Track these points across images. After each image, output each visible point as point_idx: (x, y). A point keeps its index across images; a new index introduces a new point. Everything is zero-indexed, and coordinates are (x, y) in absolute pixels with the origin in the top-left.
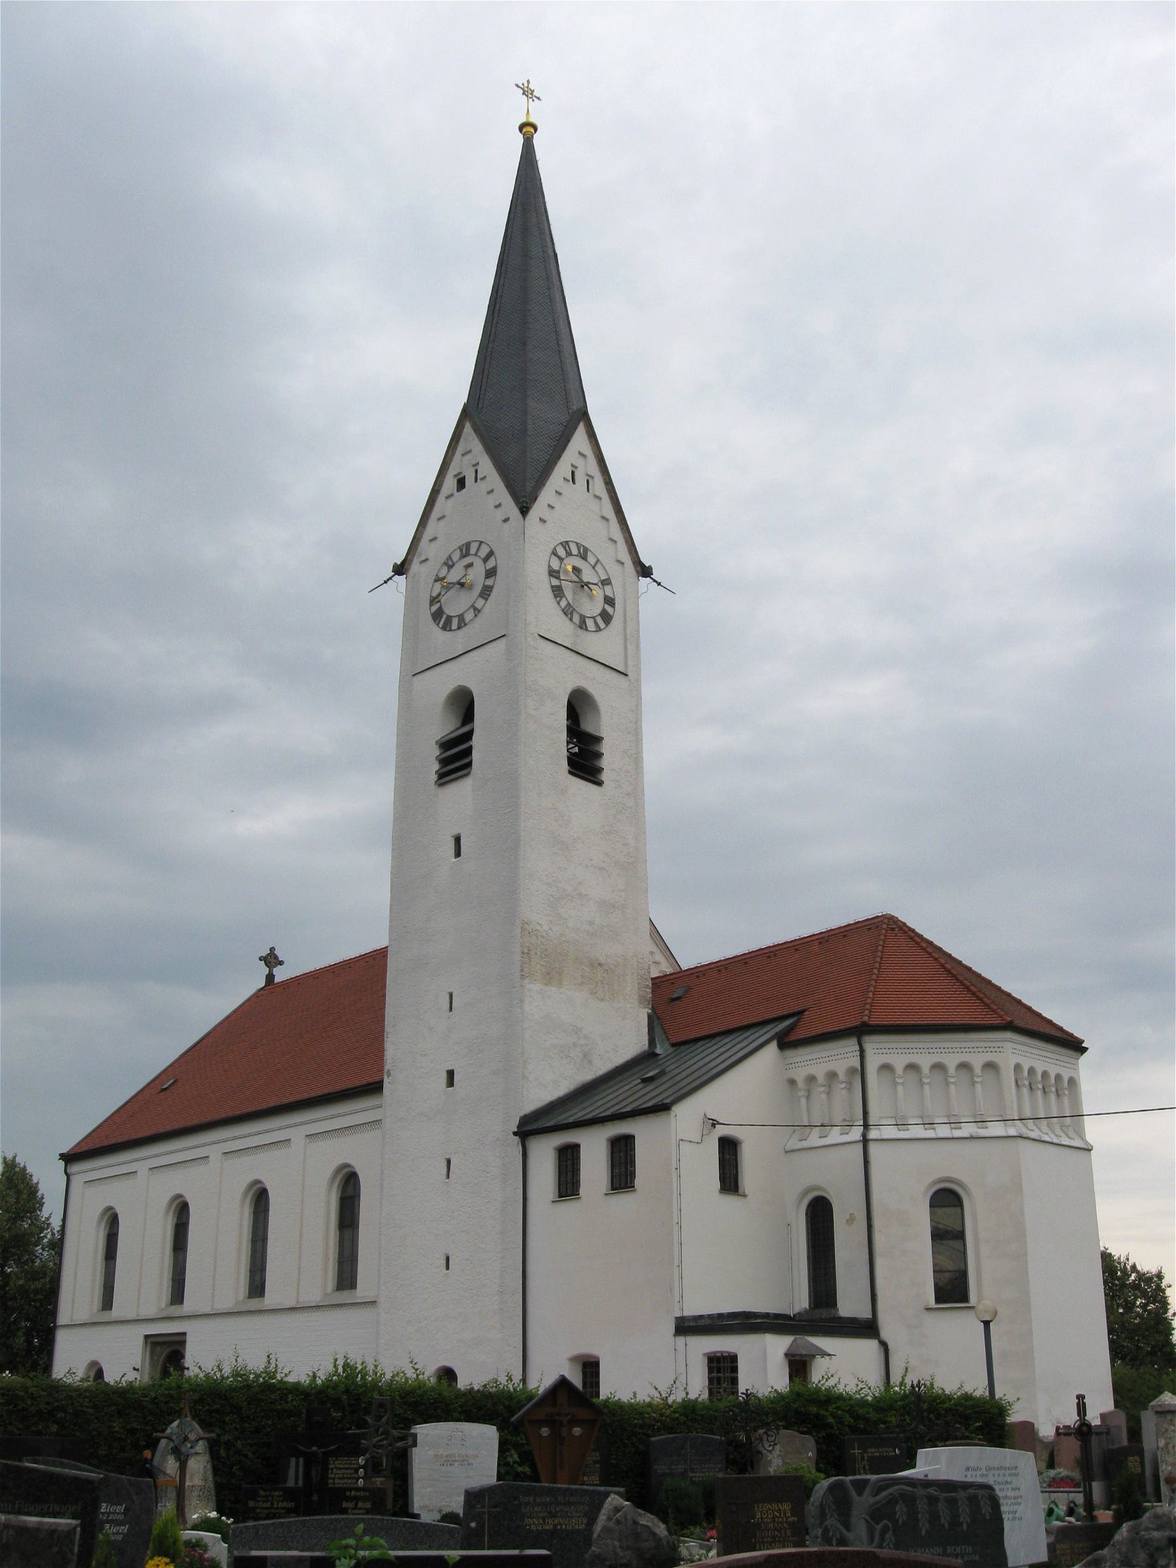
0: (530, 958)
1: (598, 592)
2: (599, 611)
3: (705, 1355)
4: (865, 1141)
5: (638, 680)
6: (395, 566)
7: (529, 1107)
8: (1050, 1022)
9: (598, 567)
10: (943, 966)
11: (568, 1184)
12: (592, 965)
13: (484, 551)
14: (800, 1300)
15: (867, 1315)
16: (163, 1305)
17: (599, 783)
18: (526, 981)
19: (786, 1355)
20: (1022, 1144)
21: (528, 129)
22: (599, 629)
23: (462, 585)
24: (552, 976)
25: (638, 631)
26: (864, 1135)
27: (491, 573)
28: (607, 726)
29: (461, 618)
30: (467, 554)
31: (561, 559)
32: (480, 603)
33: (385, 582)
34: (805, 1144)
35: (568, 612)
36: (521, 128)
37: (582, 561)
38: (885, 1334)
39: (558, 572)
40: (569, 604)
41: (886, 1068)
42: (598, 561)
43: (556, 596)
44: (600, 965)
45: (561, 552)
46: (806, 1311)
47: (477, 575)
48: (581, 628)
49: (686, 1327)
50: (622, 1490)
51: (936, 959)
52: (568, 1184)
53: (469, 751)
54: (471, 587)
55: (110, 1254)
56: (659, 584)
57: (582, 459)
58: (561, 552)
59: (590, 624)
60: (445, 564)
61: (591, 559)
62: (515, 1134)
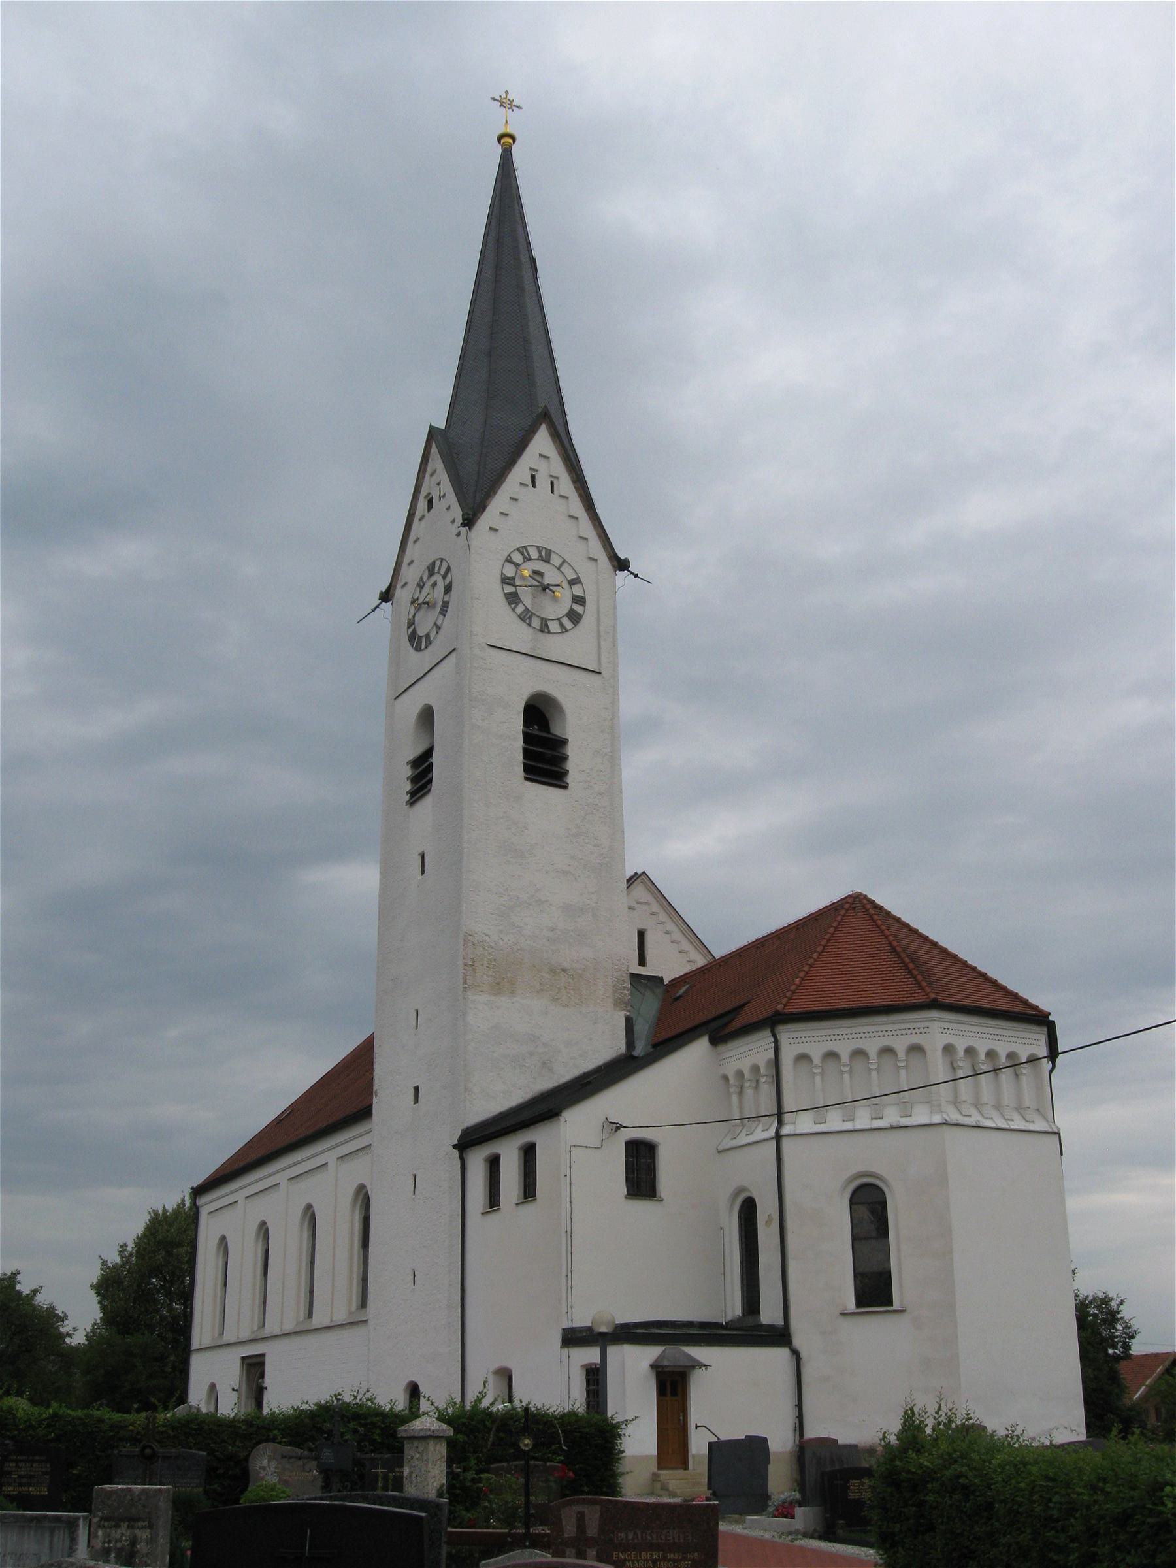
0: (474, 970)
1: (564, 596)
2: (566, 611)
3: (583, 1366)
4: (778, 1137)
5: (615, 677)
6: (381, 594)
7: (472, 1120)
8: (1015, 996)
9: (565, 568)
10: (890, 943)
12: (553, 971)
14: (734, 1309)
15: (780, 1322)
16: (354, 1308)
17: (565, 787)
18: (469, 993)
19: (652, 1366)
20: (948, 1132)
21: (506, 140)
22: (564, 630)
23: (427, 603)
24: (503, 985)
25: (614, 627)
26: (777, 1132)
27: (448, 589)
28: (576, 730)
29: (427, 636)
31: (517, 565)
33: (373, 611)
34: (734, 1143)
35: (526, 617)
36: (499, 139)
37: (545, 564)
38: (797, 1342)
39: (514, 578)
40: (527, 609)
41: (803, 1058)
42: (564, 561)
43: (510, 603)
44: (564, 970)
45: (517, 558)
46: (739, 1319)
47: (438, 594)
48: (542, 631)
49: (573, 1338)
51: (886, 937)
53: (430, 766)
54: (434, 606)
55: (312, 1262)
56: (636, 576)
57: (543, 461)
58: (517, 558)
59: (554, 627)
60: (418, 585)
61: (556, 560)
62: (455, 1147)
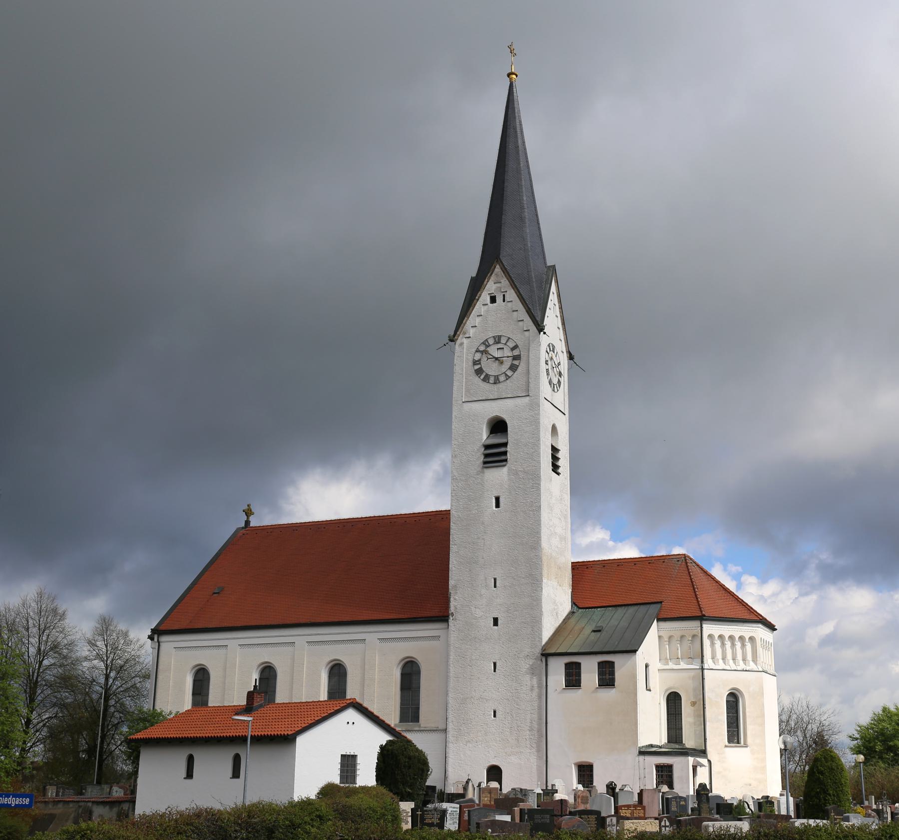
4: (703, 669)
11: (573, 679)
13: (511, 344)
27: (517, 358)
30: (499, 342)
32: (509, 373)
41: (711, 636)
50: (162, 788)
52: (573, 679)
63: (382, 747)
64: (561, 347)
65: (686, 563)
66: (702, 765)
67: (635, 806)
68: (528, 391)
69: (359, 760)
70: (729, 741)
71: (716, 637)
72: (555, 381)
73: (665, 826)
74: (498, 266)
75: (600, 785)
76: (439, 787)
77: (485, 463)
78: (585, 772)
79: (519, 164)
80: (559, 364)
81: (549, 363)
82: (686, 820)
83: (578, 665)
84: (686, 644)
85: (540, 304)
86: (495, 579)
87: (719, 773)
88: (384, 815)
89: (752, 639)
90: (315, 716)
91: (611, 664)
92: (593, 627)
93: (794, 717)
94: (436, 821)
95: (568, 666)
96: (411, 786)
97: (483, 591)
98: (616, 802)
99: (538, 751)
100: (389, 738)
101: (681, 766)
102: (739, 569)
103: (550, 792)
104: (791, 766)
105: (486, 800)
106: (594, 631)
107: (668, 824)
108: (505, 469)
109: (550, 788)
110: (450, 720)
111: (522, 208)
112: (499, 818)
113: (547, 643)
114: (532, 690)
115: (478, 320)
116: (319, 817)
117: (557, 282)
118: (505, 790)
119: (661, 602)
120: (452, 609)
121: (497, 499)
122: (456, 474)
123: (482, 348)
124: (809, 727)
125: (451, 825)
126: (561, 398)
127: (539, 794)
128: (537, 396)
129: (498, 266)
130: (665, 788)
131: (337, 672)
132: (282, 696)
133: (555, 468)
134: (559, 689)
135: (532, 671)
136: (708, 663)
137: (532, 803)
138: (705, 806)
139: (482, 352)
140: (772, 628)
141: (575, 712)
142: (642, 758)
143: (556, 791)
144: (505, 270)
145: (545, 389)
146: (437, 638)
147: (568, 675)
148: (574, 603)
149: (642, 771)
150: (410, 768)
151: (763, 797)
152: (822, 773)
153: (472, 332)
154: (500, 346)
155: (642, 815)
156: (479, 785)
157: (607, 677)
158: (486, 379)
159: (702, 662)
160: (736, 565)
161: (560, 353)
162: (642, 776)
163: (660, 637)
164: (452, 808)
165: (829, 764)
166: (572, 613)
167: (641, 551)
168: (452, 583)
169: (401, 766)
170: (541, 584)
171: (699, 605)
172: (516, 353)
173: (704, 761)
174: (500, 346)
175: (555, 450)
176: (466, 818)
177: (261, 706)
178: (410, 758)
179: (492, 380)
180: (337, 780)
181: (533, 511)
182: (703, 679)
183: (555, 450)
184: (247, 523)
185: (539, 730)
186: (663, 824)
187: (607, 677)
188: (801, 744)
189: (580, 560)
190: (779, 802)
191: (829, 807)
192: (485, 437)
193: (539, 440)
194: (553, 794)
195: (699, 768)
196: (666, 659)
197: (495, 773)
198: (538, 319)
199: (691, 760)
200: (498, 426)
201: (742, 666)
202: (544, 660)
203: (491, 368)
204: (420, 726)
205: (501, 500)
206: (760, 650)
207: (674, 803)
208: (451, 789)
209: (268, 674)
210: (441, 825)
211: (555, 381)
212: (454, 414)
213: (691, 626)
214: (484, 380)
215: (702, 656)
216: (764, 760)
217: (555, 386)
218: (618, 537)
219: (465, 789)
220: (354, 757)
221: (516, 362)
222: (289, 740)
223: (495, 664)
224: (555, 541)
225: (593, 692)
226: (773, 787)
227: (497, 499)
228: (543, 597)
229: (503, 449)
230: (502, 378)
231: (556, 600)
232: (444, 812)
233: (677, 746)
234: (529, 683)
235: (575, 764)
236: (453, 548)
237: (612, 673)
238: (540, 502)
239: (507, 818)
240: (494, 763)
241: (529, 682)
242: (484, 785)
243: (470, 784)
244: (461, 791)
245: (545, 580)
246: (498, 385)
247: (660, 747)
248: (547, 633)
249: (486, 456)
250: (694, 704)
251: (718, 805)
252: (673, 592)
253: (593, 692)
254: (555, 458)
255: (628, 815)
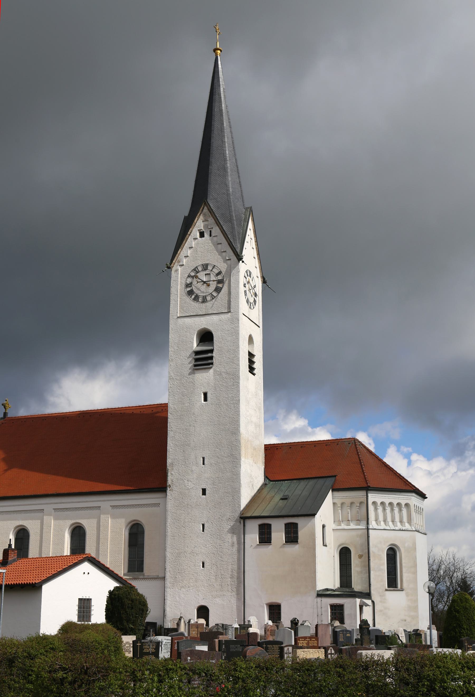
4: (368, 529)
11: (265, 537)
13: (216, 271)
32: (215, 294)
41: (374, 503)
52: (265, 537)
63: (110, 593)
64: (256, 273)
65: (356, 445)
66: (367, 605)
67: (311, 638)
68: (229, 308)
69: (93, 603)
70: (389, 587)
71: (387, 505)
72: (251, 300)
73: (331, 654)
74: (206, 208)
75: (286, 621)
76: (159, 623)
77: (195, 366)
78: (275, 611)
79: (223, 124)
80: (255, 286)
81: (247, 285)
82: (346, 649)
83: (269, 526)
84: (355, 509)
85: (239, 238)
86: (204, 458)
87: (381, 611)
88: (108, 646)
89: (407, 505)
90: (61, 567)
91: (295, 525)
92: (281, 496)
93: (443, 567)
94: (152, 650)
95: (288, 526)
96: (133, 623)
97: (194, 468)
98: (296, 634)
99: (238, 594)
100: (117, 585)
101: (351, 605)
102: (410, 449)
103: (245, 626)
104: (441, 606)
105: (194, 633)
106: (282, 499)
107: (333, 652)
108: (211, 371)
109: (246, 623)
110: (167, 570)
111: (225, 160)
112: (198, 648)
113: (245, 509)
114: (233, 546)
115: (189, 252)
116: (52, 649)
117: (253, 220)
118: (211, 624)
119: (335, 476)
120: (169, 482)
121: (205, 395)
122: (172, 374)
123: (193, 274)
124: (455, 575)
125: (164, 653)
126: (257, 314)
127: (236, 629)
128: (237, 312)
129: (206, 208)
130: (337, 623)
131: (78, 534)
132: (33, 551)
133: (251, 370)
134: (254, 545)
135: (233, 531)
136: (373, 524)
137: (231, 636)
138: (366, 638)
139: (193, 277)
140: (423, 496)
141: (265, 561)
142: (319, 599)
143: (251, 626)
144: (211, 211)
145: (243, 307)
146: (157, 505)
147: (287, 533)
148: (266, 477)
149: (319, 610)
150: (132, 608)
151: (414, 631)
152: (458, 612)
153: (185, 261)
154: (207, 272)
155: (316, 645)
156: (189, 621)
157: (292, 535)
158: (196, 299)
159: (368, 523)
160: (407, 447)
161: (255, 278)
162: (320, 614)
163: (334, 504)
164: (165, 640)
165: (464, 604)
166: (264, 485)
167: (332, 436)
168: (169, 461)
169: (125, 607)
170: (240, 462)
171: (365, 478)
172: (220, 277)
173: (369, 602)
174: (207, 272)
175: (251, 355)
176: (176, 648)
177: (14, 561)
178: (132, 601)
179: (200, 300)
180: (75, 619)
181: (234, 404)
182: (368, 537)
183: (251, 355)
184: (5, 414)
185: (238, 578)
186: (329, 652)
187: (292, 536)
188: (448, 588)
189: (296, 441)
190: (425, 634)
191: (463, 639)
192: (195, 345)
193: (238, 347)
194: (248, 628)
195: (364, 608)
196: (339, 521)
197: (203, 612)
198: (238, 250)
199: (358, 601)
200: (206, 337)
201: (399, 526)
202: (242, 522)
203: (200, 289)
204: (144, 575)
205: (209, 395)
206: (413, 514)
207: (341, 635)
208: (169, 625)
209: (22, 535)
210: (156, 654)
211: (251, 300)
212: (171, 326)
213: (359, 495)
214: (194, 299)
215: (368, 519)
216: (416, 601)
217: (251, 305)
218: (314, 424)
219: (178, 624)
220: (89, 600)
221: (220, 285)
222: (35, 588)
223: (203, 525)
224: (251, 428)
225: (281, 547)
226: (423, 622)
227: (205, 395)
228: (241, 472)
229: (210, 355)
230: (209, 298)
231: (252, 474)
232: (158, 644)
233: (348, 590)
234: (230, 541)
235: (266, 604)
236: (170, 434)
237: (296, 532)
238: (239, 397)
239: (205, 648)
240: (203, 604)
241: (231, 539)
242: (192, 622)
243: (182, 621)
244: (176, 627)
245: (243, 459)
246: (206, 304)
247: (334, 591)
248: (244, 501)
249: (196, 360)
250: (360, 556)
251: (377, 637)
252: (350, 470)
253: (281, 547)
254: (251, 362)
255: (305, 645)
